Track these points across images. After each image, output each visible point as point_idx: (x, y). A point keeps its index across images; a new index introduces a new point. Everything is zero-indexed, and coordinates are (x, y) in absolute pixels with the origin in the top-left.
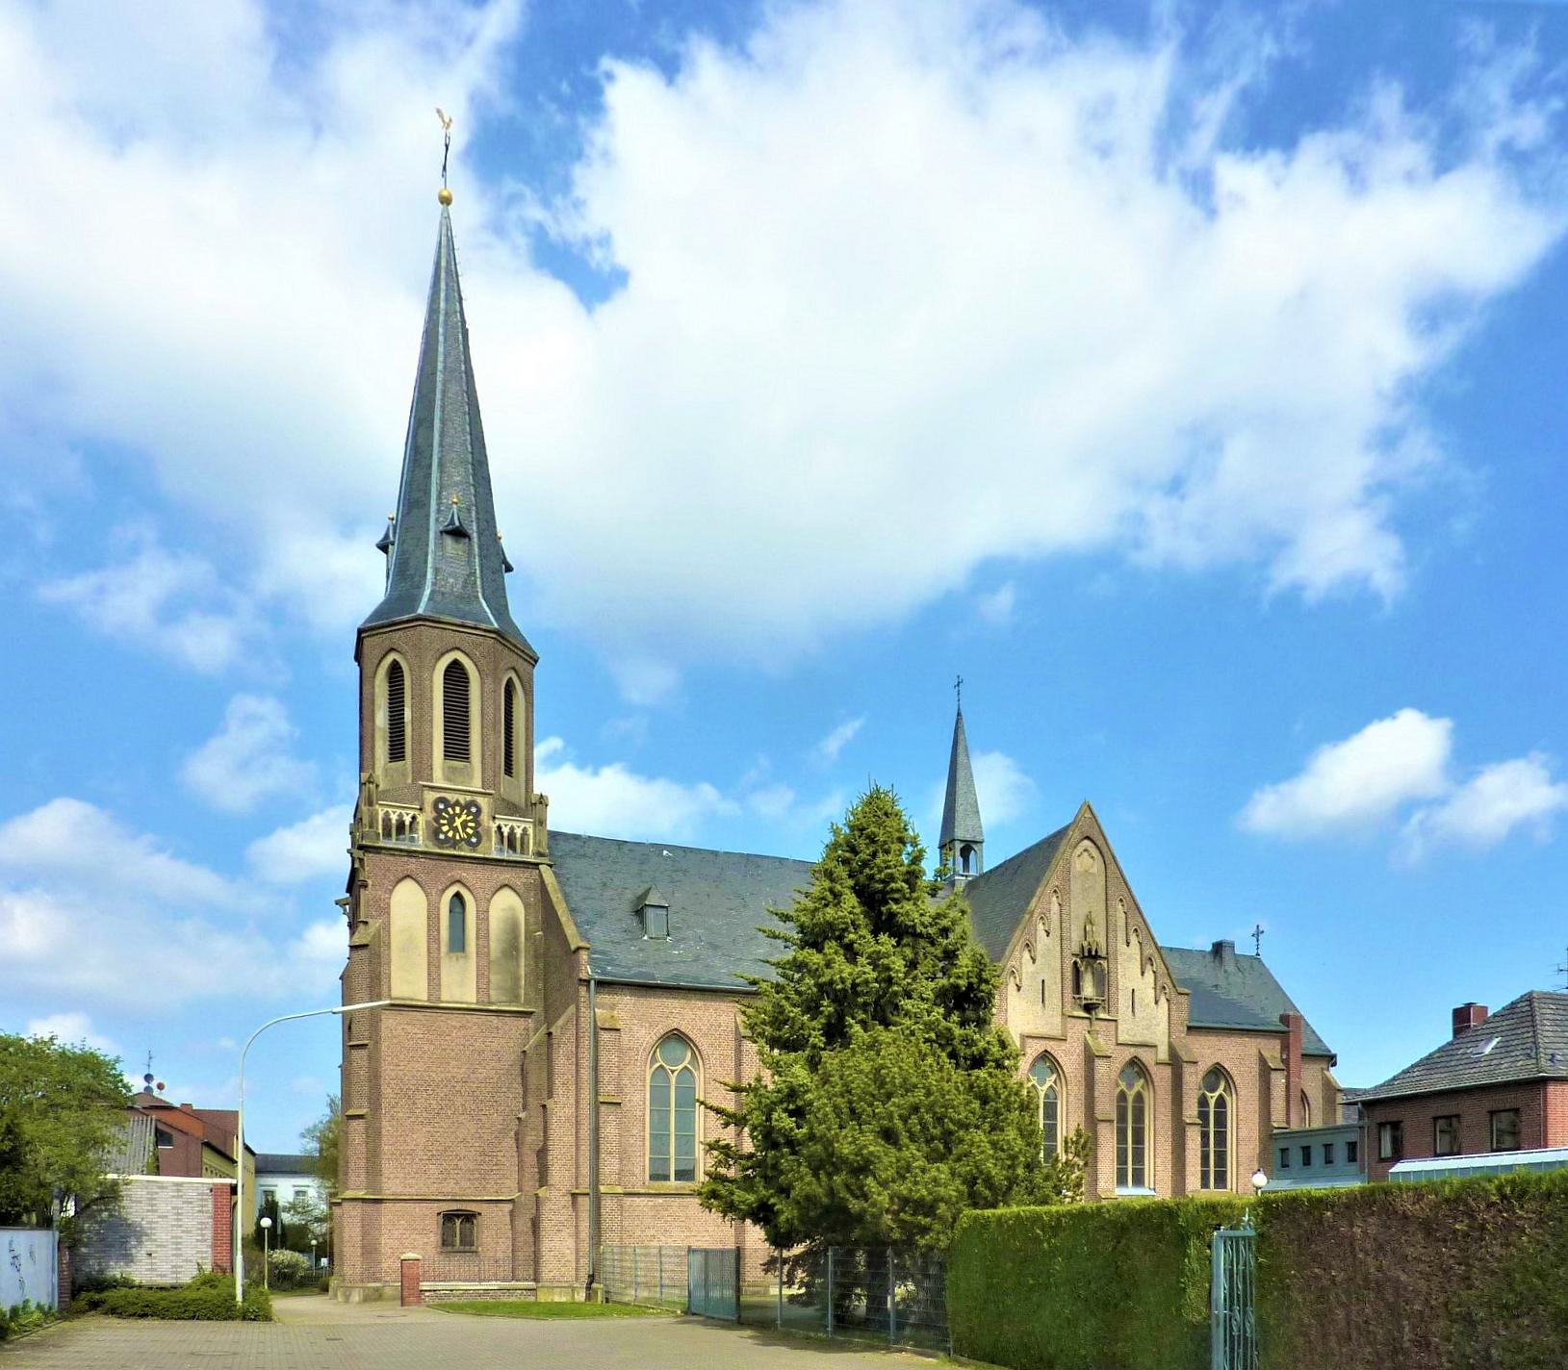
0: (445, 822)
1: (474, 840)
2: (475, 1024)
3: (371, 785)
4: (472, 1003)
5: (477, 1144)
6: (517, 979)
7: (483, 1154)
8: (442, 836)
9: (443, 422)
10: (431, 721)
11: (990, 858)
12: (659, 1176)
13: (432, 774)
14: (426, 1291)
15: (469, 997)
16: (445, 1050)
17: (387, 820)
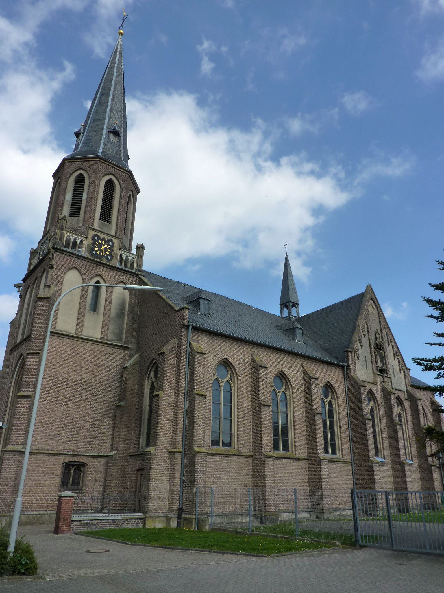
0: (97, 246)
1: (109, 257)
2: (98, 350)
3: (64, 221)
4: (98, 339)
5: (91, 420)
6: (121, 329)
7: (94, 426)
8: (94, 253)
9: (113, 96)
10: (97, 200)
11: (304, 310)
12: (215, 443)
13: (93, 224)
14: (75, 521)
15: (97, 335)
16: (80, 362)
17: (68, 240)
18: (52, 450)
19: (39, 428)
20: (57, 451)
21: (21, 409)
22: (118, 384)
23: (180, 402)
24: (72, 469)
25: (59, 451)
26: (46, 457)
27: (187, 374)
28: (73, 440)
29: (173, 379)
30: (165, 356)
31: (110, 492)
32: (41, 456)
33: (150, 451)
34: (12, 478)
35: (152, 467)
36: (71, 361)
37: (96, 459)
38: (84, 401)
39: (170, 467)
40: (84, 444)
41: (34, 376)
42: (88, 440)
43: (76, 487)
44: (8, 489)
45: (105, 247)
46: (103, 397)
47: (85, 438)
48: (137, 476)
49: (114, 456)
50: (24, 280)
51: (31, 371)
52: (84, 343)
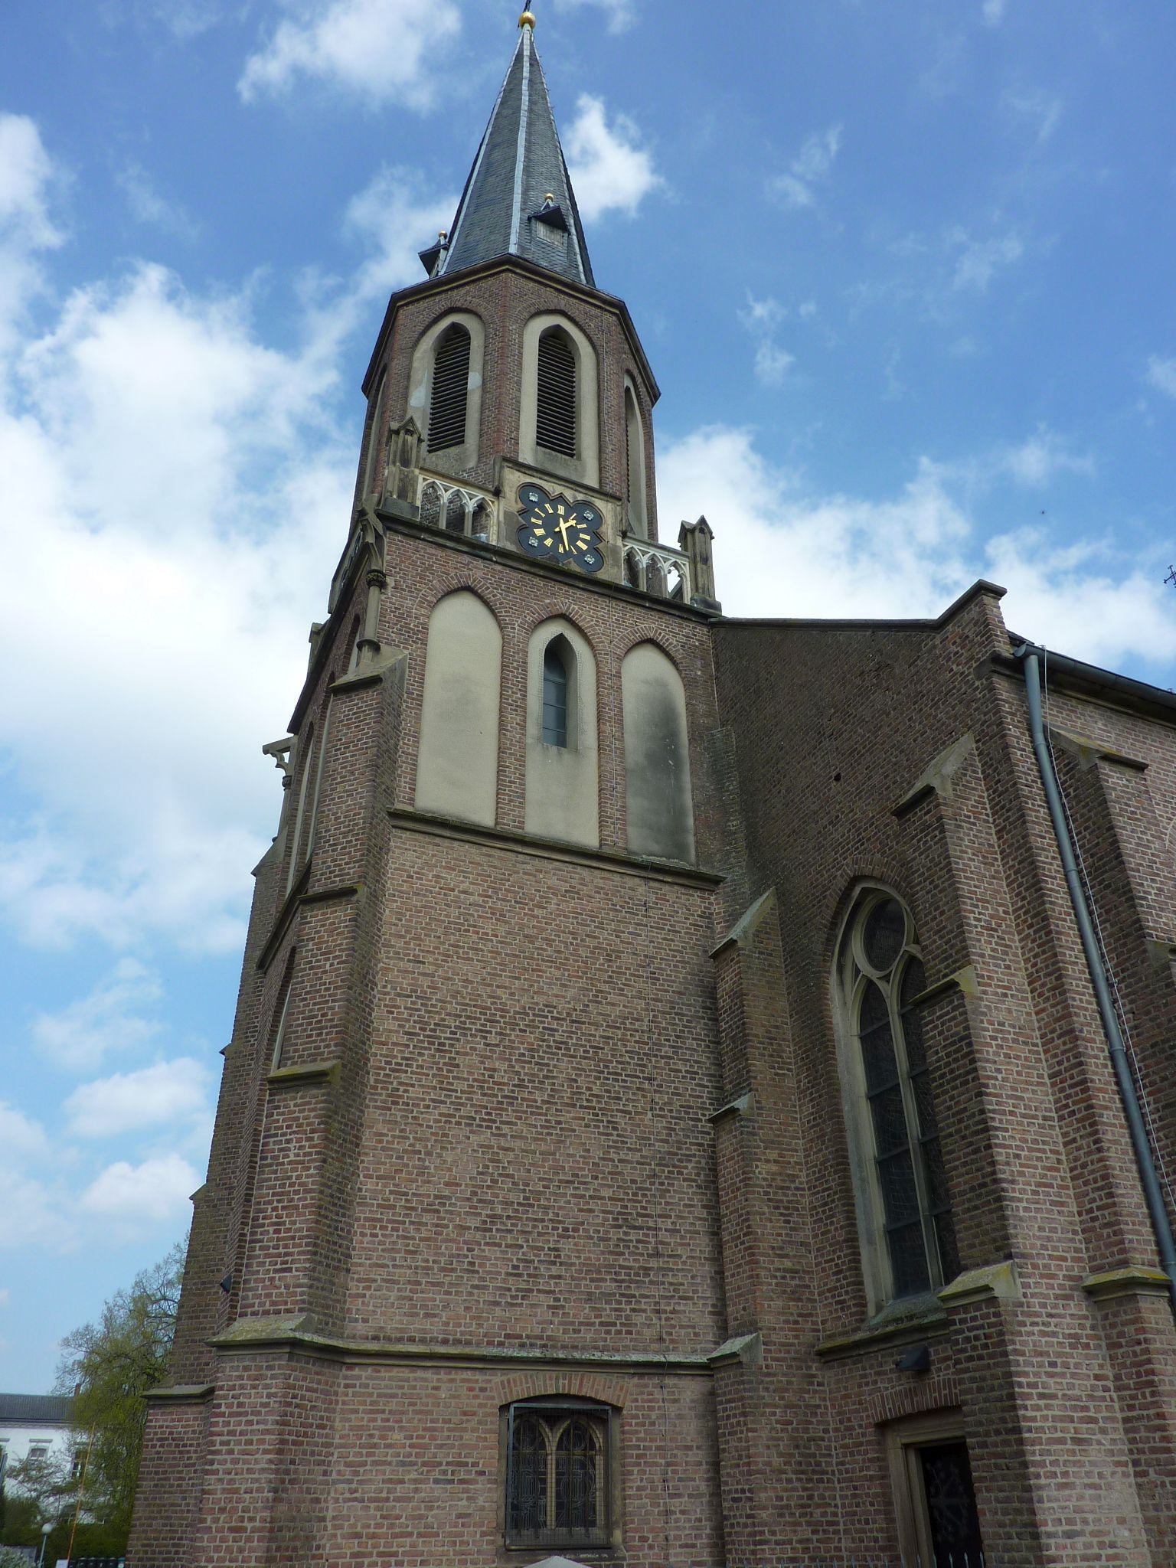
1: (590, 560)
3: (409, 438)
5: (606, 1193)
6: (678, 813)
8: (534, 542)
10: (519, 383)
16: (530, 938)
18: (445, 1342)
19: (377, 1231)
20: (468, 1343)
21: (288, 1141)
22: (699, 1028)
23: (1082, 1013)
24: (552, 1438)
25: (478, 1344)
26: (420, 1374)
27: (1074, 876)
28: (539, 1291)
29: (1001, 909)
30: (938, 805)
31: (754, 1552)
32: (395, 1372)
33: (987, 1289)
34: (259, 1490)
35: (1020, 1385)
36: (489, 931)
37: (656, 1381)
38: (568, 1105)
39: (1118, 1378)
40: (593, 1309)
41: (336, 988)
42: (609, 1286)
43: (579, 1530)
44: (241, 1550)
45: (568, 525)
46: (646, 1086)
47: (592, 1280)
48: (884, 1459)
49: (744, 1359)
50: (294, 727)
51: (325, 972)
52: (537, 861)
